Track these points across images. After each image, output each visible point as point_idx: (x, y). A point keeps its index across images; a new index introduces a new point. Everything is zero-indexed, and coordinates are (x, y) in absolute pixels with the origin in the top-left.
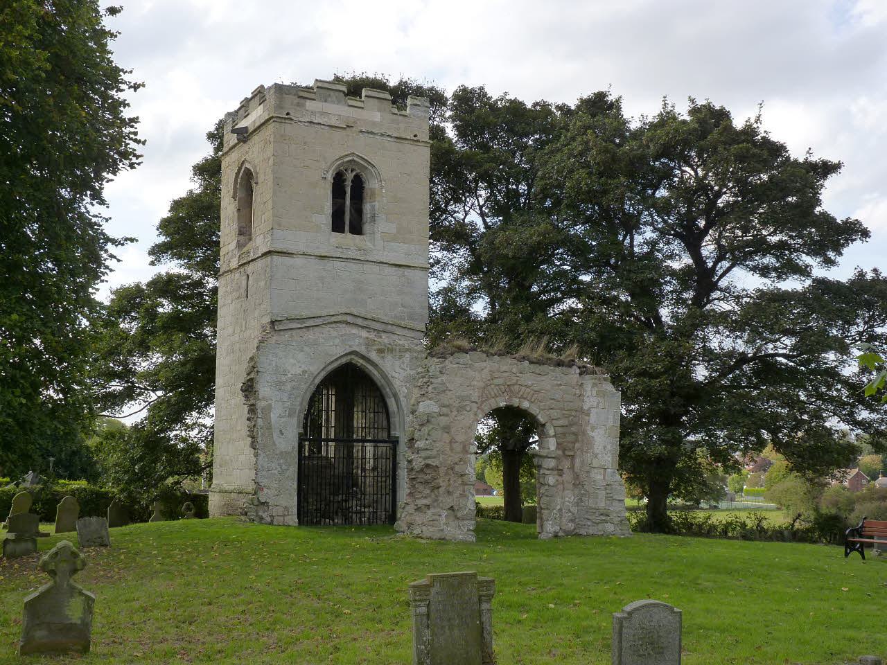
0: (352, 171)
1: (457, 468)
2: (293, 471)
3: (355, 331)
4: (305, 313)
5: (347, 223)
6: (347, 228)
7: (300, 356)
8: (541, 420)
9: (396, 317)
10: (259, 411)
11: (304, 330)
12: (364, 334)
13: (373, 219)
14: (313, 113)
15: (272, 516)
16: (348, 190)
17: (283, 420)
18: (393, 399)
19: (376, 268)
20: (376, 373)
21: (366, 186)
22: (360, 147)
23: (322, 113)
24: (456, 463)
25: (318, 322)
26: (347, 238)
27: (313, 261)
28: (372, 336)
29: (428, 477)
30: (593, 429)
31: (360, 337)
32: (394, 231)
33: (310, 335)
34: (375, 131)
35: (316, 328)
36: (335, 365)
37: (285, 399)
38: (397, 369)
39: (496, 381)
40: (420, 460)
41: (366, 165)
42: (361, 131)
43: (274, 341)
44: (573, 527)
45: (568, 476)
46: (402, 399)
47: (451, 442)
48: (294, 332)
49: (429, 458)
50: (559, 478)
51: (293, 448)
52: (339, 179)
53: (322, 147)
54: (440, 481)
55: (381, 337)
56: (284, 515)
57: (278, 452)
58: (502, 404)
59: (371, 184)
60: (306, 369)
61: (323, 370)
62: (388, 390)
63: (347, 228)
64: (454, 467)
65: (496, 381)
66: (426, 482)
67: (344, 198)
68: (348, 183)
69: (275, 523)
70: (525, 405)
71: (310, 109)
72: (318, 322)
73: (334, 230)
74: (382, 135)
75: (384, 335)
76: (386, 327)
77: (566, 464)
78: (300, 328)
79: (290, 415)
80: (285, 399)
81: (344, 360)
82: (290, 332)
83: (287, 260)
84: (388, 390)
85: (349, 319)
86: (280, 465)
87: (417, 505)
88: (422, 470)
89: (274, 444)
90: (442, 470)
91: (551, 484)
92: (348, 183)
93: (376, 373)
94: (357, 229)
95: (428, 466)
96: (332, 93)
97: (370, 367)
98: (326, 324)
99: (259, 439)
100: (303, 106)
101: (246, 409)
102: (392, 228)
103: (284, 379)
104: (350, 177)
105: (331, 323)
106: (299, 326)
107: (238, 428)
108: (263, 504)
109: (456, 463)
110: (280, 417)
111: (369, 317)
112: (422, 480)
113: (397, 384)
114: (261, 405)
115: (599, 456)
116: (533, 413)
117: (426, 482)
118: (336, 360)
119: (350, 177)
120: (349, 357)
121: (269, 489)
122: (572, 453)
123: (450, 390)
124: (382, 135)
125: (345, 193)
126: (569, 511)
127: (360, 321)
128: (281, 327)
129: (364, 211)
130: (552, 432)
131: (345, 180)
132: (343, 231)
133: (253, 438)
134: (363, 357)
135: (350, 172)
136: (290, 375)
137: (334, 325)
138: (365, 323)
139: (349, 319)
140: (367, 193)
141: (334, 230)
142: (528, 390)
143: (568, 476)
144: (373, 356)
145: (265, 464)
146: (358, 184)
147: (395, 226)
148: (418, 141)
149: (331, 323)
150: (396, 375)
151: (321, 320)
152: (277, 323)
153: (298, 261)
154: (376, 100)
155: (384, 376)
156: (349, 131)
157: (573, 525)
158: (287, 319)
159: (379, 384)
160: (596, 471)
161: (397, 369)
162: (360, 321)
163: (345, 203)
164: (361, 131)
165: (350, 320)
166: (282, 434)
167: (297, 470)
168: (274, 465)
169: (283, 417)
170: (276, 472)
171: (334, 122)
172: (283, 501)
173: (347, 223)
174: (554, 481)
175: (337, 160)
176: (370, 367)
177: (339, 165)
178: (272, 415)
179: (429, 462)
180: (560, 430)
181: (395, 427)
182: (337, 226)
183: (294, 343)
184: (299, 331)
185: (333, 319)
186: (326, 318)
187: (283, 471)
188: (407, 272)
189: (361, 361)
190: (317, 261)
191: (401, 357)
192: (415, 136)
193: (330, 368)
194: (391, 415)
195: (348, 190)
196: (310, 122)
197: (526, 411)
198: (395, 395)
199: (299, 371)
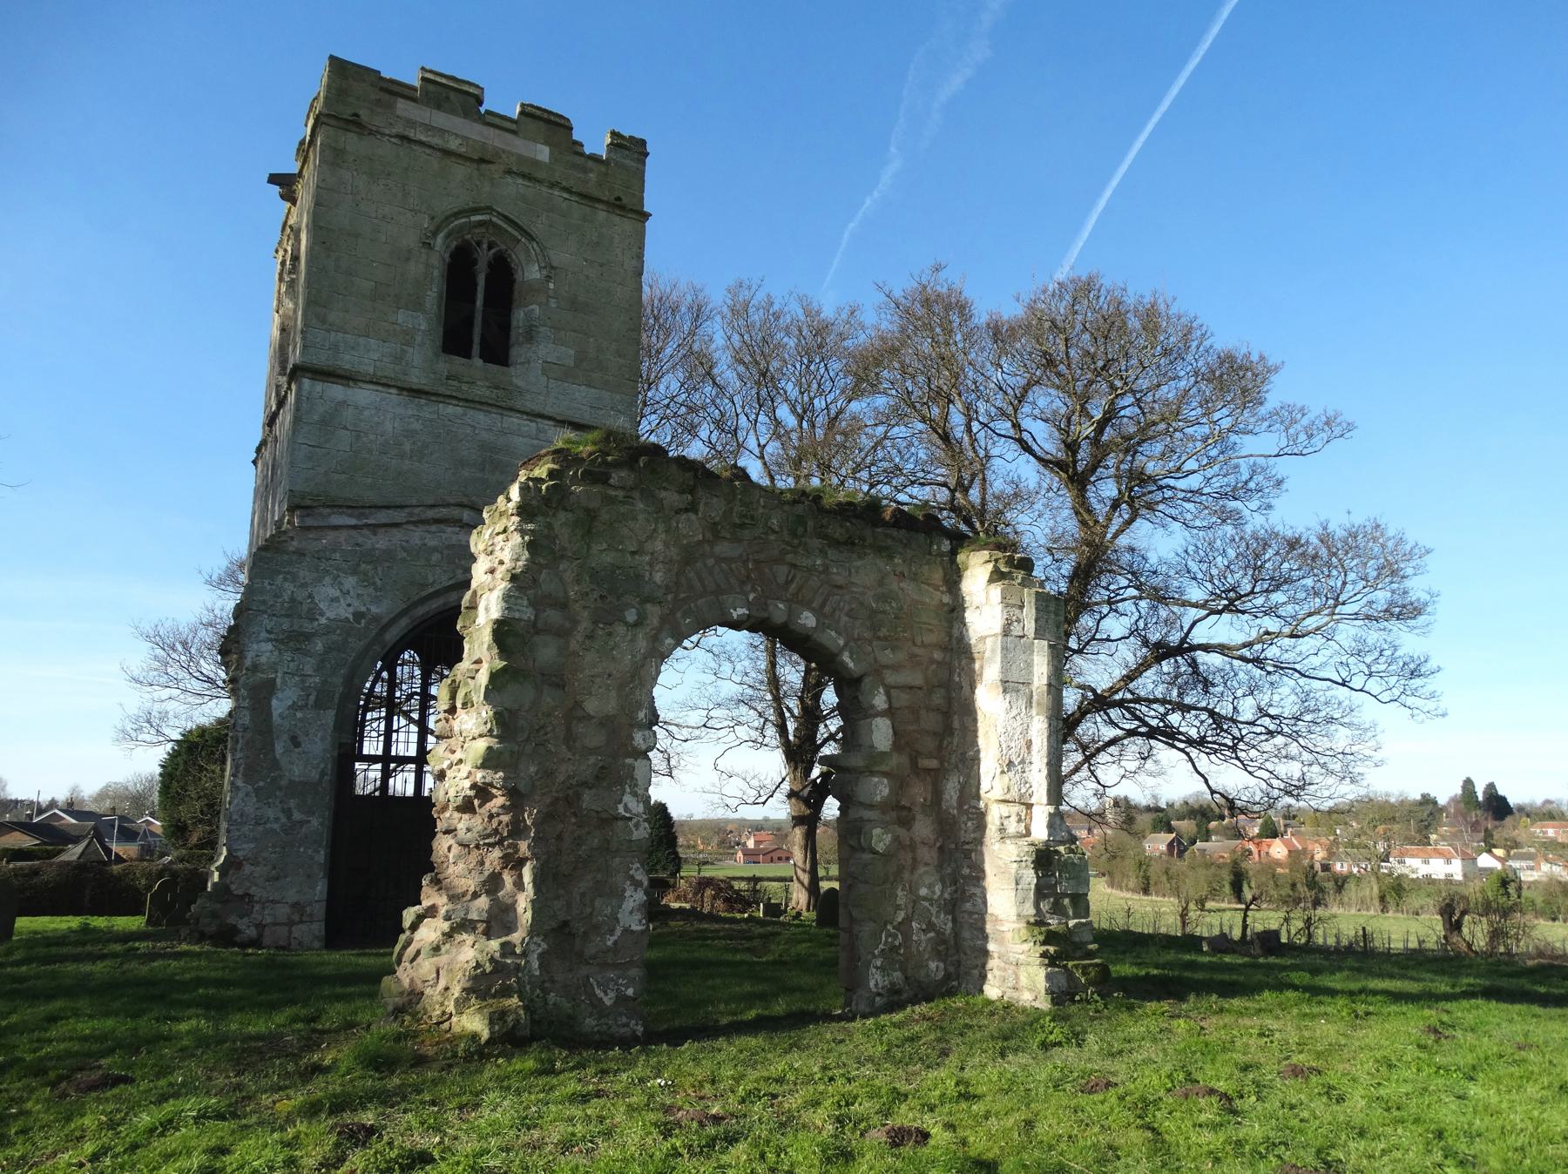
0: (490, 247)
1: (588, 800)
4: (371, 497)
5: (477, 339)
6: (476, 349)
8: (851, 665)
11: (365, 531)
14: (411, 124)
15: (260, 927)
21: (518, 277)
22: (509, 194)
23: (428, 128)
25: (399, 516)
27: (393, 396)
34: (541, 175)
35: (394, 531)
37: (308, 670)
41: (515, 233)
44: (941, 974)
45: (923, 828)
50: (902, 832)
51: (323, 774)
52: (460, 266)
56: (291, 923)
57: (283, 783)
60: (363, 609)
63: (476, 349)
64: (578, 796)
69: (267, 940)
72: (399, 516)
74: (552, 185)
77: (919, 792)
80: (308, 670)
86: (288, 813)
89: (275, 764)
91: (880, 848)
96: (452, 95)
98: (415, 523)
100: (391, 107)
102: (567, 355)
103: (308, 627)
104: (484, 257)
106: (353, 522)
110: (294, 707)
119: (484, 257)
121: (255, 863)
122: (934, 764)
126: (931, 926)
129: (514, 323)
130: (880, 701)
131: (475, 262)
132: (468, 356)
135: (485, 246)
136: (323, 621)
137: (433, 528)
143: (923, 828)
147: (572, 352)
153: (363, 395)
157: (942, 965)
166: (297, 744)
169: (301, 708)
170: (276, 826)
171: (453, 144)
173: (477, 339)
174: (888, 838)
175: (457, 215)
178: (274, 702)
180: (902, 699)
184: (353, 533)
185: (430, 514)
186: (417, 510)
190: (404, 398)
192: (618, 199)
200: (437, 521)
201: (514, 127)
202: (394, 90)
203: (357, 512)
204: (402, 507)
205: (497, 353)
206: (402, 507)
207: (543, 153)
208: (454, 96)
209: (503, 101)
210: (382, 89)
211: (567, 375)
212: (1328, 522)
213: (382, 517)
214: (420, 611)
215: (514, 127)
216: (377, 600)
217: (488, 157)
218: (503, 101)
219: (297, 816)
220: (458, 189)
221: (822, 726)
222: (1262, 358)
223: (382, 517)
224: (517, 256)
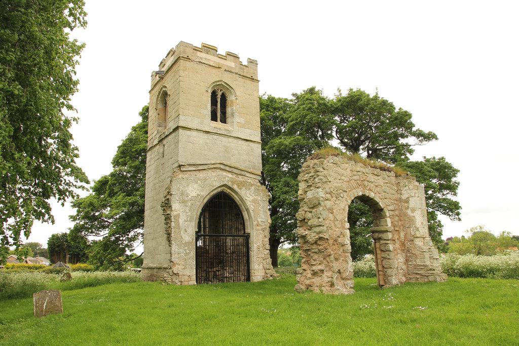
1: (340, 240)
2: (193, 253)
3: (225, 173)
7: (196, 186)
8: (381, 205)
9: (246, 167)
10: (172, 218)
12: (230, 175)
13: (233, 115)
14: (201, 58)
16: (219, 100)
17: (186, 223)
18: (246, 212)
19: (235, 141)
20: (237, 197)
22: (227, 79)
24: (339, 237)
25: (205, 167)
26: (219, 124)
27: (202, 134)
28: (234, 176)
29: (320, 248)
30: (413, 211)
31: (228, 177)
32: (243, 122)
33: (201, 175)
34: (233, 71)
36: (215, 192)
38: (248, 195)
39: (355, 178)
40: (315, 234)
42: (225, 70)
43: (180, 177)
46: (251, 211)
47: (334, 220)
48: (191, 173)
49: (320, 233)
52: (214, 94)
53: (202, 85)
54: (329, 250)
55: (238, 177)
58: (360, 194)
59: (230, 98)
61: (209, 194)
62: (243, 207)
65: (355, 178)
66: (320, 251)
67: (216, 106)
68: (219, 97)
70: (372, 195)
71: (200, 56)
72: (205, 167)
73: (212, 120)
75: (240, 177)
76: (241, 172)
78: (194, 170)
79: (190, 221)
81: (219, 190)
82: (189, 172)
83: (188, 132)
84: (243, 207)
85: (222, 167)
86: (185, 250)
87: (313, 270)
88: (316, 243)
90: (331, 242)
92: (219, 97)
93: (237, 197)
94: (224, 121)
95: (320, 238)
97: (233, 194)
99: (172, 235)
101: (163, 217)
104: (219, 94)
105: (212, 168)
107: (159, 231)
108: (175, 274)
109: (339, 237)
111: (232, 165)
112: (316, 250)
113: (248, 203)
114: (173, 214)
115: (420, 229)
116: (377, 200)
117: (320, 251)
118: (215, 189)
119: (219, 94)
120: (222, 188)
123: (330, 182)
124: (236, 74)
125: (217, 102)
127: (227, 168)
128: (184, 169)
130: (388, 214)
132: (216, 120)
133: (168, 235)
134: (230, 188)
136: (190, 197)
137: (214, 170)
138: (231, 169)
139: (222, 167)
140: (228, 102)
141: (212, 120)
142: (372, 185)
144: (235, 187)
145: (177, 250)
146: (224, 97)
148: (253, 79)
149: (212, 168)
150: (248, 199)
151: (206, 166)
152: (183, 167)
154: (232, 57)
155: (241, 199)
156: (219, 70)
158: (188, 165)
159: (238, 204)
160: (418, 239)
161: (248, 195)
162: (227, 168)
163: (217, 109)
164: (225, 70)
165: (223, 167)
166: (186, 232)
167: (195, 253)
168: (182, 250)
172: (187, 272)
176: (233, 194)
177: (214, 86)
178: (180, 220)
179: (321, 235)
181: (248, 227)
182: (214, 118)
183: (192, 178)
184: (194, 172)
187: (187, 254)
188: (251, 144)
189: (228, 190)
191: (249, 189)
193: (212, 194)
194: (245, 221)
195: (219, 100)
196: (200, 62)
197: (372, 199)
198: (247, 210)
199: (195, 195)
200: (215, 168)
201: (225, 58)
202: (196, 49)
203: (195, 166)
204: (206, 164)
205: (224, 121)
206: (206, 164)
207: (233, 65)
208: (209, 49)
209: (222, 51)
210: (194, 49)
211: (243, 126)
212: (71, 217)
213: (201, 168)
214: (212, 194)
215: (225, 58)
216: (202, 191)
217: (220, 67)
218: (222, 51)
219: (188, 251)
220: (214, 76)
221: (448, 191)
222: (304, 91)
223: (201, 168)
224: (227, 94)
